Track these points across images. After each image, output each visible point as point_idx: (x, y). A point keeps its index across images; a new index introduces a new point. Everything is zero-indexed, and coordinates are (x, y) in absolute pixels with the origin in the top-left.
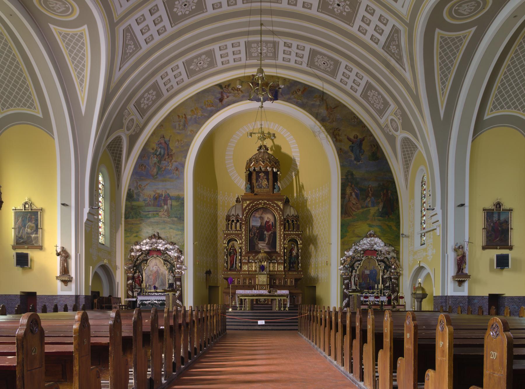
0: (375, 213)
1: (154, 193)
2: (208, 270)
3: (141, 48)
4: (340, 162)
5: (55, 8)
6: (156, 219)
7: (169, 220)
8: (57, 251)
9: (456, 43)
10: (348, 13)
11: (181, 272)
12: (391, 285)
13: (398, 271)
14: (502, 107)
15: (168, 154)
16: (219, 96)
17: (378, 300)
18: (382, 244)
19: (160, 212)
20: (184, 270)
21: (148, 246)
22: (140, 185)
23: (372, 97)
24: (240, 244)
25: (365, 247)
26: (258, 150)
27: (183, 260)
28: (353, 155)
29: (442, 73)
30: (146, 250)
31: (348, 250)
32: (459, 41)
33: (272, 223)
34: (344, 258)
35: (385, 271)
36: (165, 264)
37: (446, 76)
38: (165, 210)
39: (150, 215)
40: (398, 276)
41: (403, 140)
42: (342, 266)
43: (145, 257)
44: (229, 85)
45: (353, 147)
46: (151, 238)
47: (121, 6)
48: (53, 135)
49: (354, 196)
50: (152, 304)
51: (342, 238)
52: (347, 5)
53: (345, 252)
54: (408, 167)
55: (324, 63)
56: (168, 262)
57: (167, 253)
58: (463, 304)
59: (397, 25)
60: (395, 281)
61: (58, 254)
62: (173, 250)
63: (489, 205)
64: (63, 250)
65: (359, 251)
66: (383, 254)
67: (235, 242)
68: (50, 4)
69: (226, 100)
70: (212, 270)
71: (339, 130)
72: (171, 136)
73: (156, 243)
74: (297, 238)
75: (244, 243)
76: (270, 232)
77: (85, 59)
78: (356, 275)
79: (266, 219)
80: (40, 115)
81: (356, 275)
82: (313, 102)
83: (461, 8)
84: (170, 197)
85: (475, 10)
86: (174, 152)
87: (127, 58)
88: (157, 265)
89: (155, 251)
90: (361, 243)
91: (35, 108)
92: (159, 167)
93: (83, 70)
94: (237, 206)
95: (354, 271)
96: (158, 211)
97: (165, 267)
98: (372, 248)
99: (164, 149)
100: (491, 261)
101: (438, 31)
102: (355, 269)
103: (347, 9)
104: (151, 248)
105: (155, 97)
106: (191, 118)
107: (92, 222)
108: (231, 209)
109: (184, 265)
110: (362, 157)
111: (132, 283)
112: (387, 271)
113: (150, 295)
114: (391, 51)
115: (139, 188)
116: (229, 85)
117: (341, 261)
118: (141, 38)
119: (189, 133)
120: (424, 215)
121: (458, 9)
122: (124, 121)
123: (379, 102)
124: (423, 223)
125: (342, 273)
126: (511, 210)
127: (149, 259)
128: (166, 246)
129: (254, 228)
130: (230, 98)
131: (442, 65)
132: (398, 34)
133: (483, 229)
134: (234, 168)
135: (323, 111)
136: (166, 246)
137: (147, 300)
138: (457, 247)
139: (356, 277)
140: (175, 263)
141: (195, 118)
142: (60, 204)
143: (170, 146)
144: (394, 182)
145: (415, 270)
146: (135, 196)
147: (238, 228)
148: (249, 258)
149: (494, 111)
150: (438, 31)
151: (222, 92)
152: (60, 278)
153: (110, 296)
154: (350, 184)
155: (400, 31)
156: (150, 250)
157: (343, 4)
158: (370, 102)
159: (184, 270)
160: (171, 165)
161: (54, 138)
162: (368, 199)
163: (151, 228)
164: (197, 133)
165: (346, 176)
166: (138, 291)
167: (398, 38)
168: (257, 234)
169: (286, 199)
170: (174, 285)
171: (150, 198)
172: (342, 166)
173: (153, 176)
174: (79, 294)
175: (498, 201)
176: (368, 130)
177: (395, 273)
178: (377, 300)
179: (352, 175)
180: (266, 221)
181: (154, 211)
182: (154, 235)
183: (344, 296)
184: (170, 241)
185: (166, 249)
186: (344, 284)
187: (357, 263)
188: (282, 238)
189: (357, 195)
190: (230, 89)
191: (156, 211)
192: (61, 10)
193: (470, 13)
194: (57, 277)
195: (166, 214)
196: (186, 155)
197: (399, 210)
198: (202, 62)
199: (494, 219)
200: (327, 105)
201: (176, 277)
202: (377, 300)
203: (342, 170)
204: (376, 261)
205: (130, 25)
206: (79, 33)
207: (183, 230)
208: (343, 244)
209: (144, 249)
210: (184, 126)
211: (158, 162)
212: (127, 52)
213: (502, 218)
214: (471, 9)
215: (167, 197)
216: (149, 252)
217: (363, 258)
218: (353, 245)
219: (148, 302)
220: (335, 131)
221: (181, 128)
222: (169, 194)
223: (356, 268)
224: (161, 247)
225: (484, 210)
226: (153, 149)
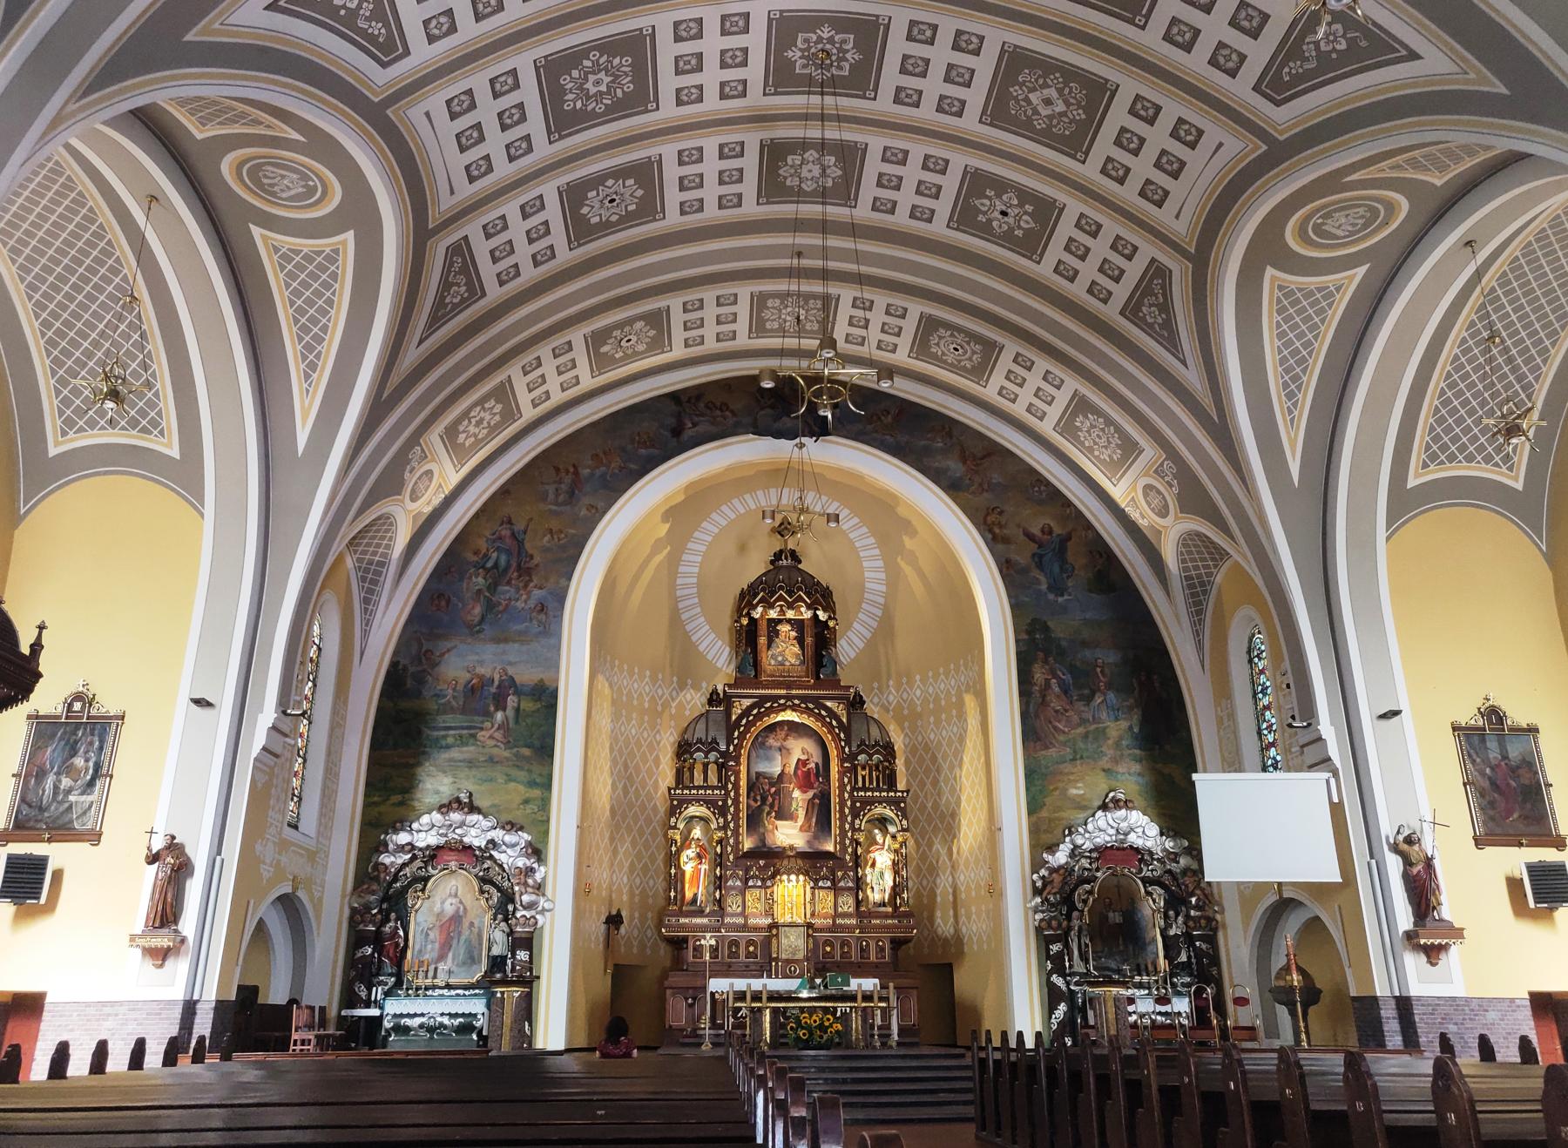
0: (1121, 738)
1: (468, 676)
2: (614, 912)
3: (484, 294)
4: (1009, 596)
5: (276, 189)
6: (469, 751)
7: (506, 754)
9: (1317, 302)
10: (1027, 232)
11: (533, 917)
12: (1193, 960)
13: (1210, 914)
14: (1452, 458)
15: (519, 567)
16: (671, 421)
17: (1167, 1008)
18: (1153, 830)
19: (482, 729)
20: (544, 911)
22: (427, 651)
23: (1088, 432)
24: (719, 828)
25: (1101, 839)
26: (772, 562)
27: (544, 879)
28: (1042, 578)
29: (1287, 371)
30: (428, 847)
31: (1052, 849)
32: (1325, 298)
33: (817, 764)
34: (1043, 872)
35: (1171, 913)
36: (482, 892)
37: (1295, 378)
39: (450, 740)
40: (1211, 930)
41: (1185, 539)
42: (1038, 900)
43: (420, 868)
44: (698, 398)
45: (1041, 557)
46: (445, 808)
47: (452, 193)
50: (431, 1030)
51: (1030, 812)
52: (1026, 213)
53: (1045, 855)
55: (956, 349)
57: (491, 857)
58: (1456, 1024)
59: (1163, 259)
60: (1204, 946)
61: (153, 859)
62: (513, 846)
63: (1467, 715)
64: (174, 847)
65: (1085, 851)
66: (1158, 860)
68: (265, 176)
69: (689, 433)
70: (624, 914)
71: (1001, 513)
72: (531, 519)
73: (462, 824)
75: (732, 825)
77: (333, 312)
78: (1085, 927)
80: (175, 453)
81: (1085, 927)
82: (923, 443)
83: (1329, 221)
84: (516, 686)
85: (1365, 226)
86: (537, 560)
87: (444, 316)
88: (456, 896)
89: (457, 850)
90: (1090, 827)
91: (162, 433)
92: (489, 600)
93: (320, 340)
94: (711, 716)
95: (1075, 914)
96: (475, 728)
97: (483, 902)
99: (508, 552)
101: (1270, 272)
103: (1027, 222)
104: (442, 841)
105: (497, 418)
106: (592, 475)
107: (276, 756)
108: (692, 726)
109: (544, 895)
110: (1070, 583)
111: (373, 953)
112: (1177, 915)
114: (1143, 319)
115: (424, 661)
116: (698, 398)
117: (1034, 882)
118: (487, 271)
119: (584, 512)
120: (1272, 745)
121: (1323, 224)
122: (407, 475)
123: (1109, 443)
124: (1272, 765)
125: (1041, 920)
129: (761, 780)
130: (700, 429)
131: (1286, 352)
132: (1164, 280)
133: (1465, 784)
134: (699, 610)
135: (955, 467)
137: (415, 1015)
139: (1085, 933)
140: (516, 888)
141: (603, 476)
142: (187, 700)
143: (528, 545)
145: (1264, 913)
146: (409, 683)
148: (747, 870)
149: (1432, 467)
150: (1270, 272)
151: (680, 413)
152: (142, 942)
153: (292, 1001)
154: (1041, 655)
155: (1171, 271)
156: (439, 848)
157: (1016, 211)
158: (1082, 443)
160: (524, 597)
161: (202, 515)
162: (1098, 699)
163: (447, 780)
164: (605, 513)
165: (1028, 632)
166: (386, 984)
167: (1163, 287)
168: (770, 799)
171: (454, 690)
172: (1016, 608)
173: (470, 627)
174: (196, 997)
176: (1079, 514)
177: (1203, 922)
178: (1163, 1009)
179: (1046, 629)
181: (462, 728)
182: (458, 800)
183: (1052, 997)
184: (505, 817)
185: (492, 842)
186: (1048, 957)
187: (1080, 890)
188: (847, 811)
189: (1062, 684)
190: (702, 405)
192: (293, 193)
193: (1352, 233)
194: (133, 938)
195: (498, 735)
198: (634, 338)
199: (1491, 756)
200: (963, 451)
201: (516, 935)
202: (1163, 1009)
205: (466, 238)
206: (328, 250)
208: (1034, 830)
209: (421, 844)
210: (572, 494)
211: (489, 588)
212: (447, 300)
214: (1354, 225)
215: (508, 685)
216: (433, 855)
217: (1099, 874)
220: (988, 514)
221: (561, 498)
222: (512, 678)
223: (1080, 906)
224: (475, 838)
225: (1454, 729)
226: (476, 553)
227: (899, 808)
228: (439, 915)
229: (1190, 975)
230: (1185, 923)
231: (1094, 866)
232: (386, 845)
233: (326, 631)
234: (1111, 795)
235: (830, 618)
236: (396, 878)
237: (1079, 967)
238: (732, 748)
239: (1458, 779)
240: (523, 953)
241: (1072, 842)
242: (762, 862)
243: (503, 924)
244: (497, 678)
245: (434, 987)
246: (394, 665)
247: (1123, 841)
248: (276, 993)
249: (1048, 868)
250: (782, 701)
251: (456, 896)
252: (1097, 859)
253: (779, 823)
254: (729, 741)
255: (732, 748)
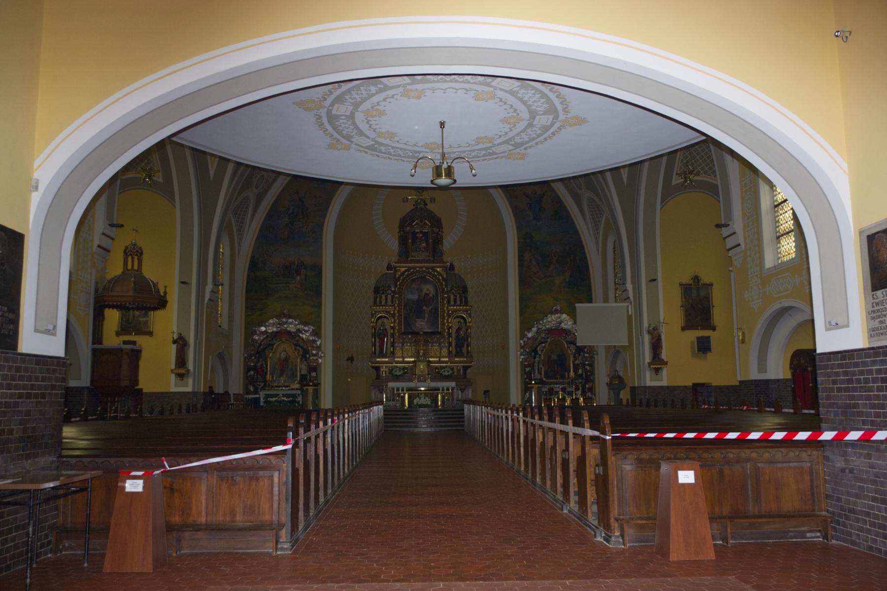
2: (350, 356)
8: (173, 338)
21: (275, 326)
27: (320, 344)
30: (273, 332)
31: (529, 330)
33: (433, 295)
34: (525, 339)
36: (296, 349)
38: (297, 282)
43: (270, 341)
46: (279, 317)
48: (175, 202)
49: (534, 263)
54: (598, 229)
56: (300, 347)
57: (299, 336)
61: (175, 342)
63: (686, 279)
65: (543, 330)
67: (385, 320)
70: (354, 356)
73: (286, 323)
74: (458, 313)
76: (430, 308)
79: (425, 291)
88: (285, 351)
90: (545, 321)
95: (537, 356)
98: (559, 326)
100: (692, 343)
102: (538, 354)
111: (254, 374)
112: (579, 355)
113: (276, 390)
126: (711, 285)
127: (275, 343)
128: (298, 327)
136: (298, 327)
138: (651, 328)
140: (310, 348)
144: (583, 247)
147: (389, 302)
152: (175, 371)
156: (276, 332)
159: (321, 357)
161: (175, 206)
169: (450, 265)
170: (308, 377)
175: (696, 274)
180: (426, 294)
182: (284, 314)
186: (525, 373)
191: (286, 283)
194: (172, 371)
196: (326, 215)
197: (589, 279)
203: (518, 232)
204: (565, 343)
207: (319, 306)
209: (270, 331)
213: (702, 293)
216: (275, 335)
218: (535, 323)
219: (274, 399)
224: (292, 328)
227: (467, 313)
228: (280, 358)
229: (582, 379)
230: (582, 359)
231: (547, 336)
232: (256, 332)
233: (224, 248)
234: (555, 308)
235: (439, 231)
236: (260, 345)
237: (537, 376)
238: (396, 289)
239: (680, 304)
240: (314, 373)
241: (537, 327)
242: (410, 336)
243: (305, 362)
244: (296, 262)
245: (279, 387)
246: (253, 257)
247: (559, 326)
248: (219, 389)
249: (527, 338)
250: (418, 269)
251: (285, 351)
252: (548, 334)
253: (417, 320)
254: (396, 286)
255: (396, 289)
